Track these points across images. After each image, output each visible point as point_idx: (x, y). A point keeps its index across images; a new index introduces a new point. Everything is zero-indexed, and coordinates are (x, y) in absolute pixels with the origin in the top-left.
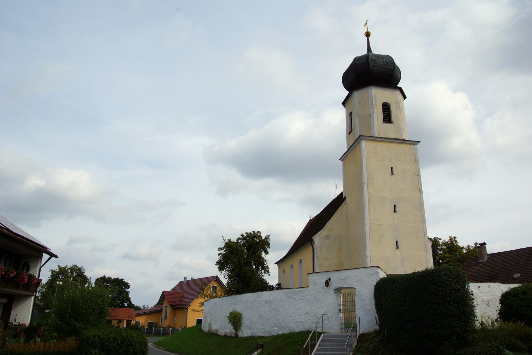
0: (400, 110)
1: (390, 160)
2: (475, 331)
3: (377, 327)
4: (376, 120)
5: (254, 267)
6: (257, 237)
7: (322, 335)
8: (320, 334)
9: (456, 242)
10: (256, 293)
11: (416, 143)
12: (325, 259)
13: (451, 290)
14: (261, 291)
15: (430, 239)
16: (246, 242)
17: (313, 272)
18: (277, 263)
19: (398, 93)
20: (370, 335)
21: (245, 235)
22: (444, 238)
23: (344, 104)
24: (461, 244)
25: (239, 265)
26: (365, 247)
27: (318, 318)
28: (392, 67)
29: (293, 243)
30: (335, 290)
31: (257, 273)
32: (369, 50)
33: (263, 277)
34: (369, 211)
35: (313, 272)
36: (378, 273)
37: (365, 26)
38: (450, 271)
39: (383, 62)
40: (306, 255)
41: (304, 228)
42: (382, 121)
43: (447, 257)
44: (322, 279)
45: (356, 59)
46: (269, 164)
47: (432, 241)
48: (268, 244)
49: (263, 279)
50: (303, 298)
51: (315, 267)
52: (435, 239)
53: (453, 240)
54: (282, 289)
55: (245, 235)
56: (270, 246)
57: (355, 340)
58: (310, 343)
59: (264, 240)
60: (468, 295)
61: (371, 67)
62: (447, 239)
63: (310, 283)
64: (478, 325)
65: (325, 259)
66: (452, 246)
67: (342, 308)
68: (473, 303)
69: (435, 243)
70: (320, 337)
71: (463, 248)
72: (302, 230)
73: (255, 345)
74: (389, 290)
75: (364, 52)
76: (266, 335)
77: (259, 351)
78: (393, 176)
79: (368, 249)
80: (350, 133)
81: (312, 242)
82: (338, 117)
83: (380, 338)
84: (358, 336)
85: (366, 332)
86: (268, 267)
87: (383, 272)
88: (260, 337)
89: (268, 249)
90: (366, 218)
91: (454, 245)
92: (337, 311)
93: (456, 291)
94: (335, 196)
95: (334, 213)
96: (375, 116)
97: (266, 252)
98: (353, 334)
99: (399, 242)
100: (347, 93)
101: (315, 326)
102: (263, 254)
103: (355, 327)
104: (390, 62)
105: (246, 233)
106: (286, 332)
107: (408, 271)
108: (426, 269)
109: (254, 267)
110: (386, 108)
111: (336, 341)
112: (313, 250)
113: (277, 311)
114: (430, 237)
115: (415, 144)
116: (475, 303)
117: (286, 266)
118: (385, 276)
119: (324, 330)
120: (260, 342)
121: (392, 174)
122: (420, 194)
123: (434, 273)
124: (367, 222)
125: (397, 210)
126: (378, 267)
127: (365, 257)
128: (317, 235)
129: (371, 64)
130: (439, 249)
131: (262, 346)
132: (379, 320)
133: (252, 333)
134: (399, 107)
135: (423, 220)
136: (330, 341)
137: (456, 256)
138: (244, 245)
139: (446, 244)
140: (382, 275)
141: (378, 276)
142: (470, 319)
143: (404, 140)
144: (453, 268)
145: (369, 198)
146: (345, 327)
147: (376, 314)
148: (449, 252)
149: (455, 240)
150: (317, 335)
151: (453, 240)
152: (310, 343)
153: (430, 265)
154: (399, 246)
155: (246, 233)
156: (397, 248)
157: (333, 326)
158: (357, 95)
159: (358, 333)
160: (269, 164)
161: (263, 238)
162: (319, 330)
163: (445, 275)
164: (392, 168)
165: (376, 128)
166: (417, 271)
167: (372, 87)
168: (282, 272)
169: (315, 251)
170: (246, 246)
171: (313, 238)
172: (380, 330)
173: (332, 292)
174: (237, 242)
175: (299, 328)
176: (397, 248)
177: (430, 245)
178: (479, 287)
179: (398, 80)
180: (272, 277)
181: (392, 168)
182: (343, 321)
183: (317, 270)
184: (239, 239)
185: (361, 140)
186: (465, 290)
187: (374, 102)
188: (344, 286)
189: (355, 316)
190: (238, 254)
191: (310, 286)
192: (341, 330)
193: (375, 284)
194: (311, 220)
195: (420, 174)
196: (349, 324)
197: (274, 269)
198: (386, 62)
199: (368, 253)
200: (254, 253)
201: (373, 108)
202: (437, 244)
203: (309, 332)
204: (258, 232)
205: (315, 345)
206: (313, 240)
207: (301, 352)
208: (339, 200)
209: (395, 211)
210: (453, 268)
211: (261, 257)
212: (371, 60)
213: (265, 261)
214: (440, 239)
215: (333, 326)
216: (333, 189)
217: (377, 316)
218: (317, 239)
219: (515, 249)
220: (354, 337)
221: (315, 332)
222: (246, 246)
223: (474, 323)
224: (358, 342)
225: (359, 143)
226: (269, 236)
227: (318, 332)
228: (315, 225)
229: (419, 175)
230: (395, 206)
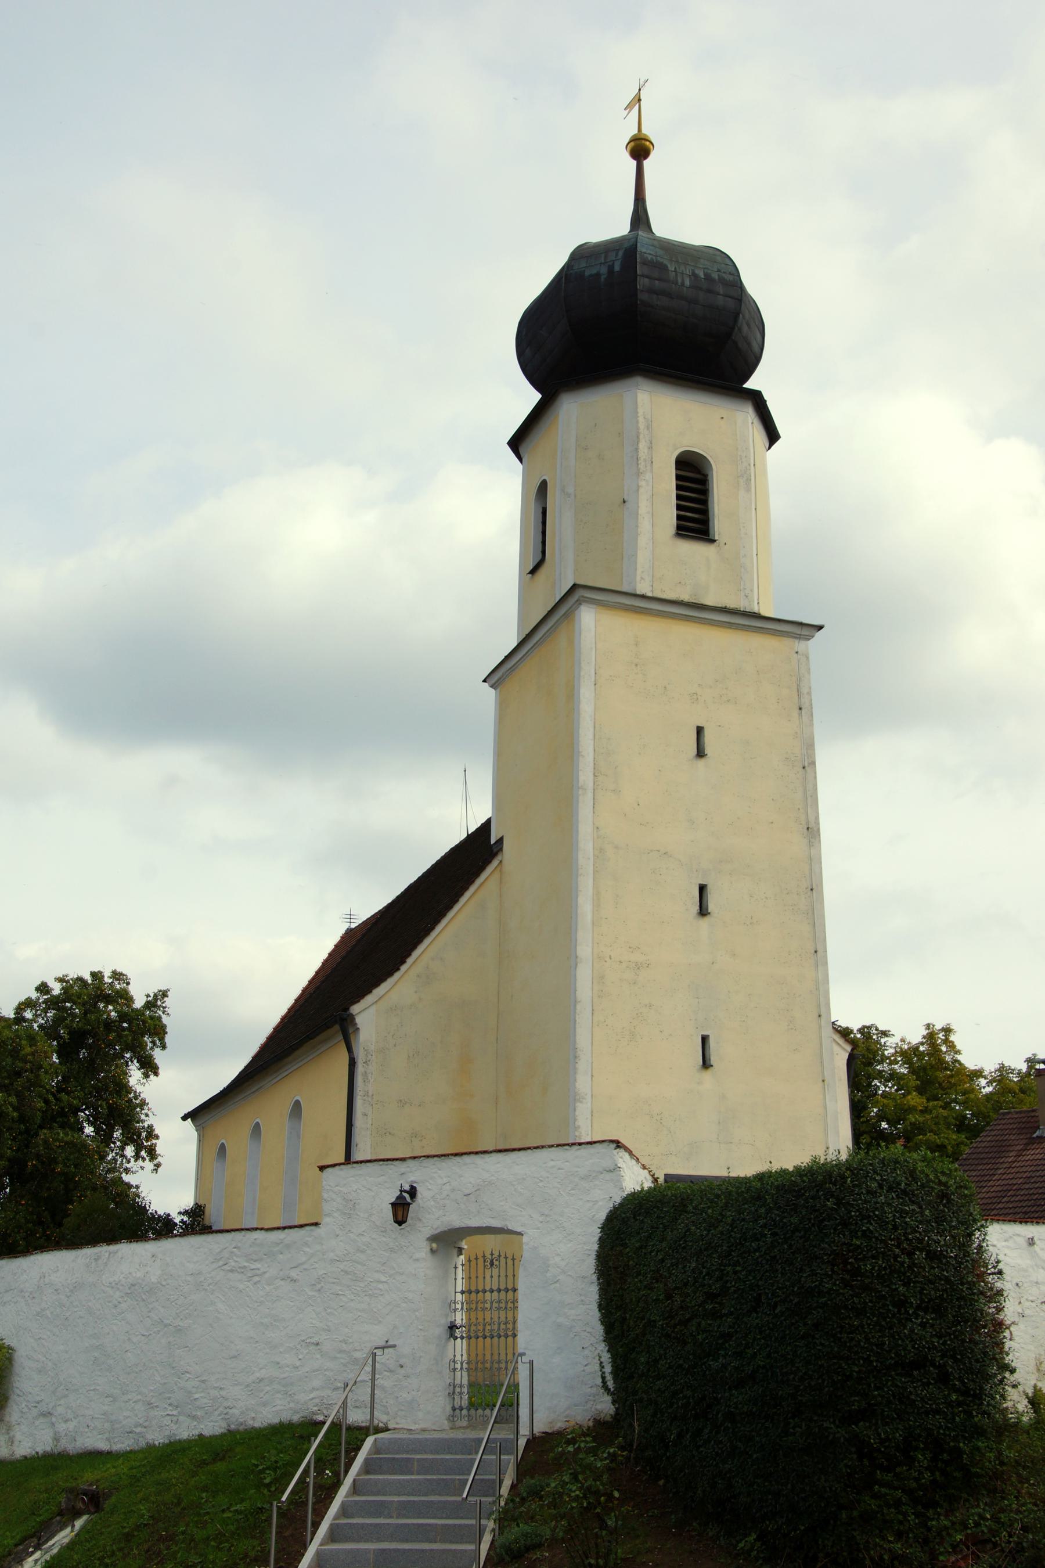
0: (748, 490)
1: (695, 698)
2: (1006, 1428)
3: (605, 1406)
4: (645, 524)
5: (89, 1130)
6: (108, 999)
7: (369, 1441)
8: (358, 1434)
9: (952, 1046)
10: (88, 1253)
11: (808, 630)
12: (402, 1103)
13: (910, 1254)
14: (112, 1238)
15: (845, 1033)
16: (58, 1021)
17: (348, 1159)
18: (192, 1115)
19: (747, 414)
20: (572, 1441)
21: (57, 989)
22: (904, 1028)
23: (516, 443)
24: (969, 1060)
25: (22, 1119)
26: (571, 1057)
27: (355, 1361)
28: (731, 304)
29: (268, 1030)
30: (434, 1238)
31: (102, 1157)
32: (640, 217)
33: (126, 1178)
34: (597, 904)
35: (348, 1159)
36: (617, 1168)
37: (629, 107)
38: (912, 1173)
39: (694, 275)
40: (317, 1083)
41: (317, 964)
42: (672, 530)
43: (911, 1109)
44: (379, 1190)
45: (582, 255)
46: (176, 685)
47: (854, 1043)
48: (159, 1031)
49: (129, 1186)
50: (294, 1274)
51: (358, 1137)
52: (866, 1031)
53: (937, 1042)
54: (207, 1230)
55: (57, 989)
56: (168, 1039)
57: (510, 1462)
58: (310, 1480)
59: (139, 1012)
60: (981, 1276)
61: (643, 297)
62: (915, 1036)
63: (326, 1207)
64: (1023, 1405)
65: (402, 1103)
66: (933, 1065)
67: (459, 1318)
68: (999, 1309)
69: (863, 1051)
70: (358, 1449)
71: (978, 1074)
72: (304, 983)
73: (62, 1499)
74: (670, 1251)
75: (620, 227)
76: (121, 1445)
77: (79, 1523)
78: (701, 762)
79: (582, 1065)
80: (533, 572)
81: (346, 1027)
82: (490, 505)
83: (613, 1457)
84: (522, 1442)
85: (559, 1426)
86: (151, 1134)
87: (637, 1168)
88: (94, 1457)
89: (158, 1055)
90: (580, 935)
91: (941, 1061)
92: (441, 1330)
93: (933, 1256)
94: (457, 837)
95: (449, 907)
96: (644, 507)
97: (149, 1067)
98: (504, 1433)
99: (712, 1043)
100: (534, 397)
101: (338, 1398)
102: (135, 1075)
103: (511, 1405)
104: (722, 281)
105: (61, 980)
106: (212, 1427)
107: (745, 1166)
108: (815, 1161)
109: (89, 1130)
110: (693, 477)
111: (426, 1467)
112: (352, 1063)
113: (179, 1330)
114: (843, 1023)
115: (800, 637)
116: (1010, 1311)
117: (234, 1128)
118: (648, 1184)
119: (381, 1418)
120: (88, 1479)
121: (700, 754)
122: (811, 845)
123: (843, 1177)
124: (584, 950)
125: (711, 907)
126: (618, 1144)
127: (570, 1098)
128: (369, 999)
129: (642, 283)
130: (880, 1075)
131: (94, 1501)
132: (615, 1373)
133: (57, 1439)
134: (748, 478)
135: (817, 953)
136: (403, 1466)
137: (946, 1106)
138: (49, 1031)
139: (909, 1054)
140: (634, 1179)
141: (618, 1183)
142: (988, 1377)
143: (757, 616)
144: (924, 1159)
145: (600, 853)
146: (471, 1405)
147: (602, 1347)
148: (921, 1091)
149: (946, 1041)
150: (345, 1438)
151: (937, 1042)
152: (310, 1480)
153: (834, 1139)
154: (713, 1059)
155: (61, 980)
156: (706, 1064)
157: (418, 1402)
158: (576, 409)
159: (524, 1431)
160: (176, 685)
161: (139, 1003)
162: (357, 1417)
163: (890, 1189)
164: (700, 731)
165: (643, 557)
166: (775, 1167)
167: (639, 380)
168: (213, 1156)
169: (360, 1069)
170: (58, 1037)
171: (355, 1009)
172: (617, 1417)
173: (422, 1249)
174: (19, 1019)
175: (268, 1411)
176: (706, 1064)
177: (841, 1055)
178: (1031, 1242)
179: (750, 362)
180: (166, 1185)
181: (700, 731)
182: (463, 1378)
183: (357, 1156)
184: (28, 1004)
185: (579, 603)
186: (967, 1254)
187: (643, 446)
188: (474, 1223)
189: (518, 1355)
190: (18, 1074)
191: (326, 1220)
192: (452, 1418)
193: (602, 1216)
194: (349, 932)
195: (813, 763)
196: (488, 1391)
197: (177, 1140)
198: (708, 277)
199: (583, 1083)
200: (91, 1067)
201: (638, 474)
202: (875, 1053)
203: (312, 1426)
204: (117, 975)
205: (337, 1485)
206: (352, 1018)
207: (269, 1520)
208: (476, 853)
209: (703, 911)
210: (924, 1159)
211: (122, 1087)
212: (645, 263)
213: (143, 1103)
214: (885, 1033)
215: (418, 1402)
216: (445, 809)
217: (606, 1357)
218: (369, 1014)
219: (420, 874)
220: (505, 1447)
221: (336, 1426)
222: (58, 1037)
223: (1003, 1397)
224: (523, 1470)
225: (569, 615)
226: (165, 994)
227: (350, 1428)
228: (369, 955)
229: (808, 766)
230: (702, 889)
